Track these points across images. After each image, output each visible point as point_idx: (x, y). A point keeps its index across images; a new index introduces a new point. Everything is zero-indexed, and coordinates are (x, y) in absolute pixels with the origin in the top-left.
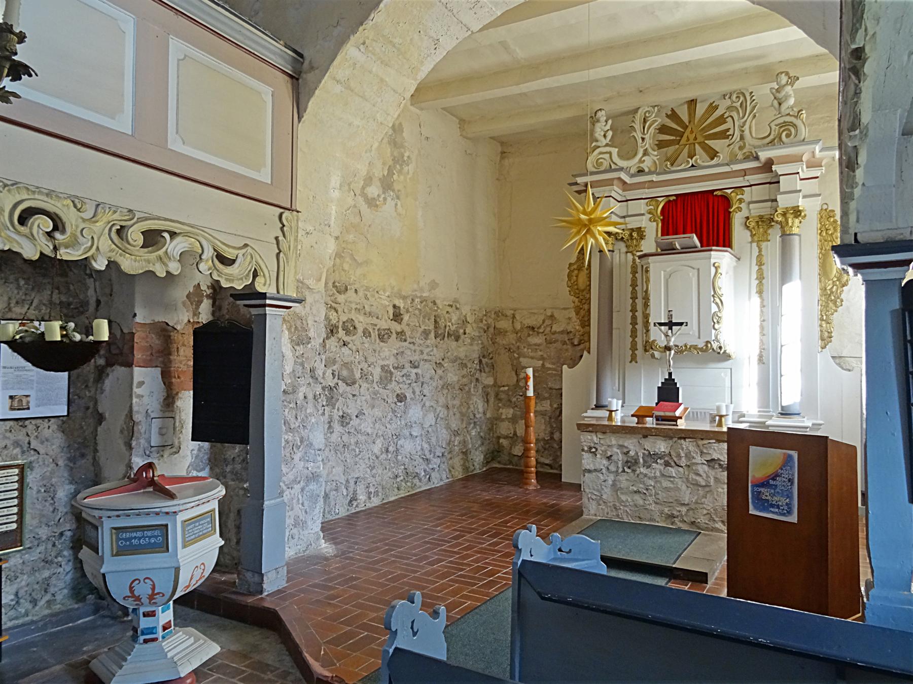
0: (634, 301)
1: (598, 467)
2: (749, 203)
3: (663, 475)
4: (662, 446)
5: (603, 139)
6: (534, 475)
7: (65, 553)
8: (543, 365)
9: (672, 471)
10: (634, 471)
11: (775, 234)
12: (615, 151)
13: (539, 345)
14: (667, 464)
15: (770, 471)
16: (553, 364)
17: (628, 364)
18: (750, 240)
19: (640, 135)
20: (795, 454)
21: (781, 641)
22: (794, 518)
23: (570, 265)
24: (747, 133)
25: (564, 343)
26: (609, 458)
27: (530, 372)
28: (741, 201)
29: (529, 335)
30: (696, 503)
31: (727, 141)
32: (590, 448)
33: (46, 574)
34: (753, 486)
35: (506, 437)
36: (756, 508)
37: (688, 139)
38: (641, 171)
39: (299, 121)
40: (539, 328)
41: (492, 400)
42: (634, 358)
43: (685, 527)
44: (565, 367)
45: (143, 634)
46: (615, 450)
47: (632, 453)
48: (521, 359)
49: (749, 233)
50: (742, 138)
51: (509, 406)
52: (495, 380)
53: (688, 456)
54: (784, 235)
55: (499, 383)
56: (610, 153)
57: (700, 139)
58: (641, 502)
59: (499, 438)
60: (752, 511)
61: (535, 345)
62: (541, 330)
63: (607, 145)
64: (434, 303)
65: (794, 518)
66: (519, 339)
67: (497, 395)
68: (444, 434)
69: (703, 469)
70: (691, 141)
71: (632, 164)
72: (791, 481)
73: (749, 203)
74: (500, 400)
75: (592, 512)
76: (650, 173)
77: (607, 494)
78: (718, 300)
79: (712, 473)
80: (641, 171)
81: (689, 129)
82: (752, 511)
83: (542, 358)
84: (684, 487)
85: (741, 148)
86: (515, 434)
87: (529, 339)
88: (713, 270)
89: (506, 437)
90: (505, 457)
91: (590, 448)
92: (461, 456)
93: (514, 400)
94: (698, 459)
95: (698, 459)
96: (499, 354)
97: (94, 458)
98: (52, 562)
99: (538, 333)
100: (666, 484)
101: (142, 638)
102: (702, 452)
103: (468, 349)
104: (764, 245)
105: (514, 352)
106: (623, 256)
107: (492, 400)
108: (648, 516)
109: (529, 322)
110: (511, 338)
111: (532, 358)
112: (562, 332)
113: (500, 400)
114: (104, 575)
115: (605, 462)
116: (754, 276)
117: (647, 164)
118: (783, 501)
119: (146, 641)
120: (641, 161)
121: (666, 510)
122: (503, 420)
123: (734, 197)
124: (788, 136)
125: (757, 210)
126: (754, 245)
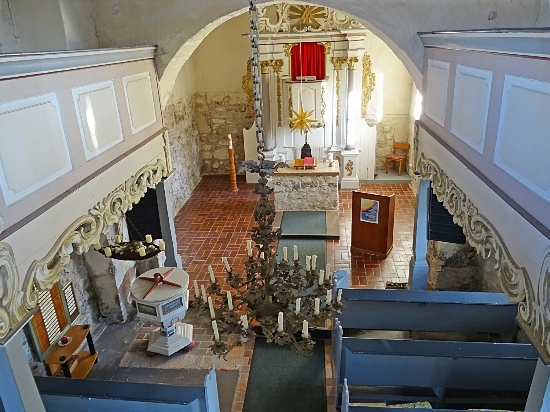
0: (279, 97)
1: (281, 190)
2: (334, 50)
3: (310, 191)
4: (309, 180)
5: (261, 13)
6: (236, 185)
7: (88, 307)
8: (226, 122)
9: (314, 189)
10: (297, 190)
11: (345, 66)
12: (268, 20)
13: (222, 112)
14: (312, 186)
15: (368, 207)
16: (231, 121)
17: (277, 127)
18: (333, 68)
19: (281, 11)
20: (378, 202)
21: (412, 300)
22: (377, 222)
23: (244, 77)
24: (334, 17)
25: (236, 111)
26: (286, 186)
27: (230, 136)
28: (329, 48)
29: (216, 107)
30: (324, 200)
31: (324, 20)
32: (277, 183)
33: (85, 319)
34: (363, 211)
35: (208, 160)
36: (363, 219)
37: (305, 17)
38: (281, 31)
39: (159, 81)
40: (221, 103)
41: (198, 141)
42: (280, 125)
43: (319, 210)
44: (244, 129)
45: (169, 333)
46: (289, 182)
47: (296, 183)
48: (213, 120)
49: (333, 65)
50: (332, 19)
51: (208, 144)
52: (199, 131)
53: (321, 183)
54: (349, 70)
55: (201, 132)
56: (266, 21)
57: (311, 17)
58: (301, 202)
59: (204, 160)
60: (361, 220)
61: (220, 112)
62: (223, 104)
63: (264, 17)
64: (173, 105)
65: (377, 222)
66: (210, 109)
67: (200, 139)
68: (185, 170)
69: (326, 187)
70: (307, 17)
71: (277, 27)
72: (376, 210)
73: (334, 50)
74: (203, 141)
75: (279, 208)
76: (286, 32)
77: (286, 200)
78: (323, 104)
79: (330, 188)
80: (281, 31)
81: (306, 11)
82: (361, 220)
83: (225, 119)
84: (319, 195)
85: (331, 24)
86: (213, 157)
87: (216, 109)
88: (322, 90)
89: (208, 160)
90: (209, 169)
91: (277, 183)
92: (192, 177)
93: (211, 140)
94: (325, 184)
95: (325, 184)
96: (199, 117)
97: (85, 262)
98: (85, 313)
99: (221, 105)
100: (311, 194)
101: (168, 335)
102: (326, 181)
103: (186, 123)
104: (340, 71)
105: (208, 116)
106: (272, 74)
107: (198, 141)
108: (304, 207)
109: (216, 99)
110: (206, 108)
111: (219, 119)
112: (235, 105)
113: (203, 141)
114: (162, 323)
115: (284, 188)
116: (335, 86)
117: (285, 27)
118: (373, 217)
119: (170, 335)
120: (281, 25)
121: (311, 204)
122: (205, 151)
123: (327, 47)
124: (354, 23)
125: (337, 54)
126: (335, 71)
